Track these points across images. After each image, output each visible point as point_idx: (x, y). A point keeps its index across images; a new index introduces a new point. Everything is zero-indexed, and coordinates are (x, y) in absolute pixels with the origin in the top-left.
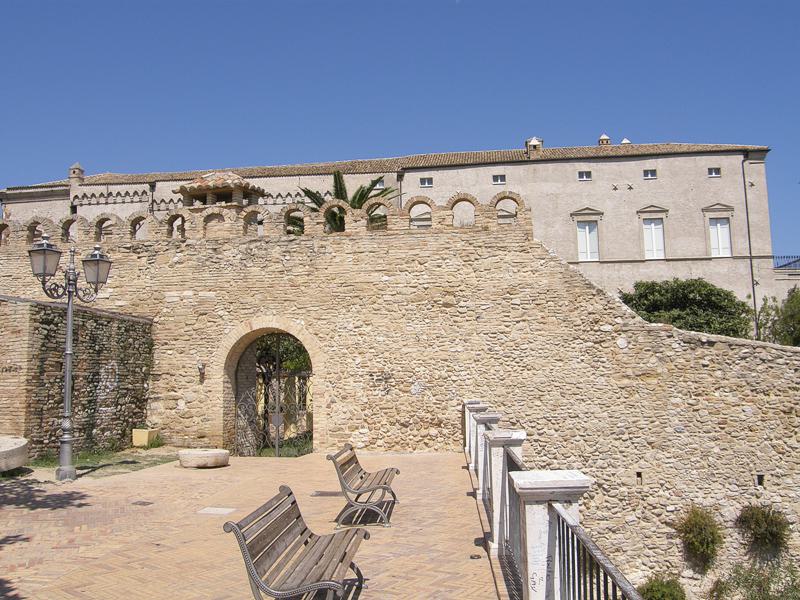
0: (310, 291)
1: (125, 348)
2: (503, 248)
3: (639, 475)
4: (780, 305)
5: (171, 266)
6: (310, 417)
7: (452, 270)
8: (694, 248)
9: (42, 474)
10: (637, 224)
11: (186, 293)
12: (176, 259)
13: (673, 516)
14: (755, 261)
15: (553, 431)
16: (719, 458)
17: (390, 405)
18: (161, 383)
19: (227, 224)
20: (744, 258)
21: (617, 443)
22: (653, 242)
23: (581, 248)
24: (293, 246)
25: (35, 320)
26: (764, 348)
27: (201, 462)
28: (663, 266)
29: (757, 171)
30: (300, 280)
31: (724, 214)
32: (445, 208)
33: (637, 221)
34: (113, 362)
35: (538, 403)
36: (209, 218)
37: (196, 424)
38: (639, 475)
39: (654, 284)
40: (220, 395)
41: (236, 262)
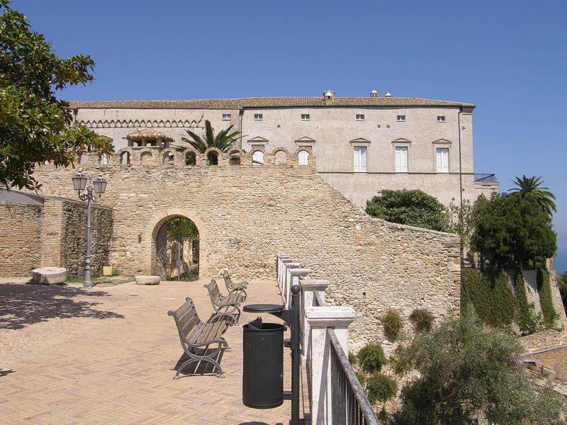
0: (199, 196)
1: (100, 224)
2: (301, 177)
3: (364, 294)
4: (472, 204)
5: (123, 180)
6: (69, 317)
7: (273, 187)
8: (426, 167)
9: (70, 285)
11: (131, 195)
12: (125, 176)
13: (380, 314)
14: (463, 176)
15: (322, 271)
18: (117, 242)
19: (154, 157)
21: (354, 278)
22: (401, 161)
23: (356, 163)
24: (190, 172)
25: (64, 210)
26: (428, 232)
27: (148, 282)
28: (407, 177)
29: (467, 119)
31: (446, 146)
32: (271, 155)
34: (95, 231)
35: (315, 257)
36: (143, 154)
37: (136, 264)
38: (364, 294)
39: (392, 192)
41: (159, 179)
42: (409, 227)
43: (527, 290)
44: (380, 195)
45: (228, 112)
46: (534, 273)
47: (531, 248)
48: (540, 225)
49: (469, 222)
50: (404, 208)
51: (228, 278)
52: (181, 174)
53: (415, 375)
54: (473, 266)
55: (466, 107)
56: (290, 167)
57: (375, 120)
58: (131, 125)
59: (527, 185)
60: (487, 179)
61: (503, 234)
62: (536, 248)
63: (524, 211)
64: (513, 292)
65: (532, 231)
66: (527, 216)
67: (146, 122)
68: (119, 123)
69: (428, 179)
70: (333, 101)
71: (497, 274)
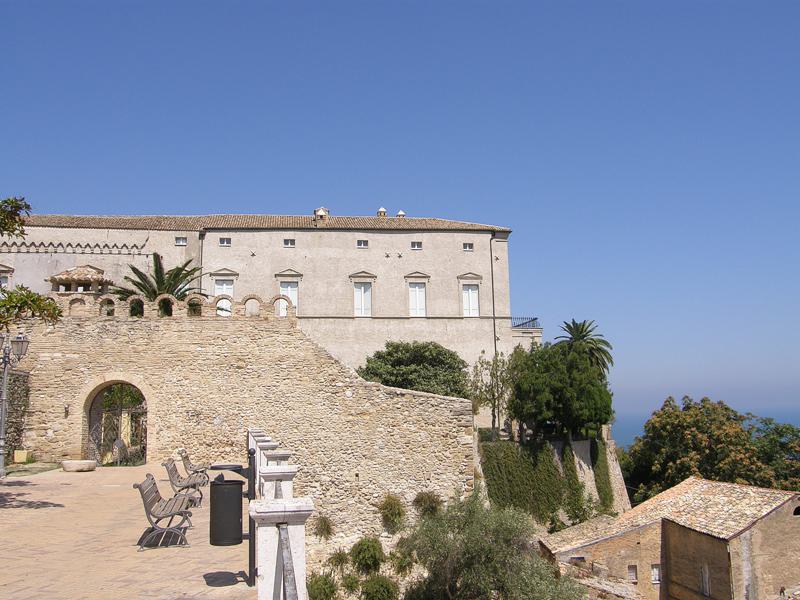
3: (357, 475)
4: (506, 359)
5: (45, 335)
7: (243, 345)
10: (403, 287)
11: (55, 355)
12: (48, 330)
14: (497, 321)
16: (405, 464)
17: (199, 432)
18: (35, 418)
19: (87, 306)
20: (489, 318)
21: (344, 456)
24: (136, 325)
27: (80, 468)
28: (425, 323)
29: (501, 248)
30: (140, 348)
31: (475, 282)
33: (404, 284)
36: (73, 302)
37: (61, 447)
38: (357, 475)
40: (80, 426)
42: (410, 391)
43: (578, 466)
44: (385, 350)
45: (183, 234)
46: (587, 444)
47: (580, 412)
48: (590, 383)
49: (503, 381)
50: (411, 367)
51: (186, 459)
52: (124, 328)
53: (420, 572)
54: (512, 439)
55: (500, 232)
56: (263, 319)
57: (382, 248)
58: (42, 249)
59: (578, 331)
60: (528, 324)
61: (546, 396)
62: (586, 412)
63: (571, 366)
64: (561, 470)
65: (582, 391)
66: (575, 372)
67: (65, 246)
68: (24, 246)
69: (452, 325)
70: (327, 221)
71: (540, 447)
